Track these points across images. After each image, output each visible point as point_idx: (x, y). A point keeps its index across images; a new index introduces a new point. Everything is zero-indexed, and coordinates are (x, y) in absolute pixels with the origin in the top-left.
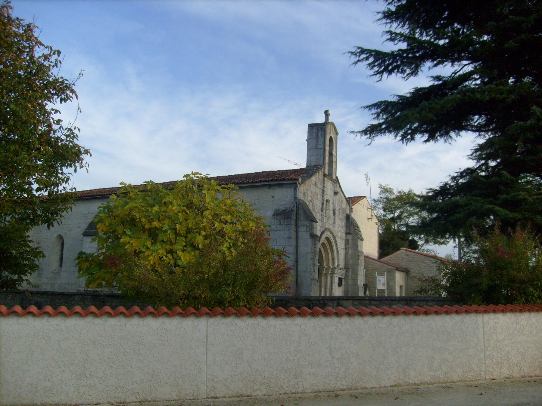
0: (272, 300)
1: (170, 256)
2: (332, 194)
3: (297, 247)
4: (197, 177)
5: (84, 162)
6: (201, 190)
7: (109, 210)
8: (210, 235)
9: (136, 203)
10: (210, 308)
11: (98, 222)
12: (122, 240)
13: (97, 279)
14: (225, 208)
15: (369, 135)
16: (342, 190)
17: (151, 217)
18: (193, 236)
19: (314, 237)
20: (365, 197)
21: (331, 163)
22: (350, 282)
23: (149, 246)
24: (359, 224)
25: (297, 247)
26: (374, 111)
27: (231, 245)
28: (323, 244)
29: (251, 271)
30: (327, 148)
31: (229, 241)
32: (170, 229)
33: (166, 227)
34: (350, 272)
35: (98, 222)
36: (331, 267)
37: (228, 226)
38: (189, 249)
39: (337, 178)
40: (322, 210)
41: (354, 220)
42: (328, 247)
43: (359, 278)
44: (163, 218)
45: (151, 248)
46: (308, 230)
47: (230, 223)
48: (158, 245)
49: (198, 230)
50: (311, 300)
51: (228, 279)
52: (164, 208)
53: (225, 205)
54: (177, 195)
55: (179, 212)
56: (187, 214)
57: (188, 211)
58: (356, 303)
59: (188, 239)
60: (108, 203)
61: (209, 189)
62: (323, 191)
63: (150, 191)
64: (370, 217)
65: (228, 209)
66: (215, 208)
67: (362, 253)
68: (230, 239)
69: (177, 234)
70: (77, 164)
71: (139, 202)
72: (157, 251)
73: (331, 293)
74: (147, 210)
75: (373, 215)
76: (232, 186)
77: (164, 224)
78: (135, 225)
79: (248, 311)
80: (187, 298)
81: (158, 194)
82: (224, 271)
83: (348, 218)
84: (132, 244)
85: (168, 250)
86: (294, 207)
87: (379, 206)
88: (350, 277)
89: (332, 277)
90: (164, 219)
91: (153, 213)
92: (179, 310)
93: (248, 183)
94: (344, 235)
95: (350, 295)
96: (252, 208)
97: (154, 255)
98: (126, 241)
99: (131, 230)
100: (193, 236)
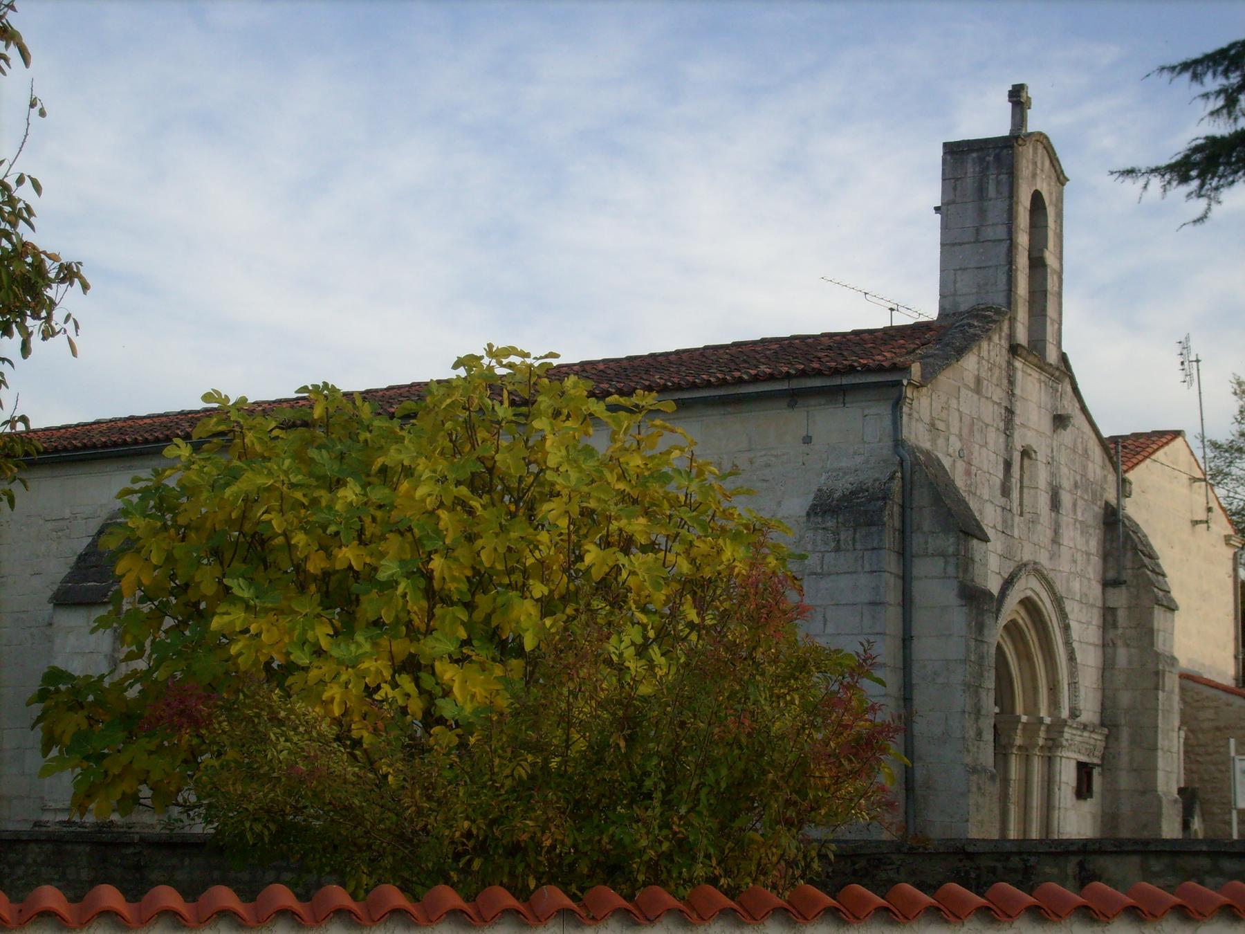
0: (822, 857)
1: (406, 681)
2: (1046, 424)
3: (907, 640)
4: (510, 366)
5: (58, 316)
6: (527, 416)
7: (161, 501)
8: (565, 599)
9: (270, 473)
10: (573, 888)
11: (122, 551)
12: (216, 623)
13: (120, 777)
14: (621, 486)
15: (1195, 184)
16: (1084, 409)
17: (332, 529)
18: (500, 600)
19: (976, 599)
20: (1177, 434)
21: (1042, 298)
22: (1125, 781)
23: (324, 643)
24: (1157, 544)
25: (907, 640)
26: (1213, 83)
27: (651, 634)
28: (1012, 629)
29: (736, 740)
30: (1023, 239)
31: (643, 618)
32: (409, 575)
33: (389, 569)
34: (1125, 734)
35: (122, 551)
36: (1048, 720)
37: (639, 560)
38: (481, 652)
39: (1064, 358)
40: (1006, 491)
41: (1136, 528)
42: (1032, 637)
43: (1161, 764)
44: (378, 531)
45: (335, 652)
46: (951, 570)
47: (644, 549)
48: (359, 638)
49: (517, 578)
50: (971, 856)
51: (646, 774)
52: (379, 494)
53: (623, 476)
54: (432, 441)
55: (441, 505)
56: (471, 512)
57: (475, 503)
58: (1156, 865)
59: (479, 615)
60: (157, 473)
61: (556, 414)
62: (1010, 412)
63: (322, 425)
64: (1201, 515)
65: (635, 493)
66: (585, 489)
67: (1173, 660)
68: (644, 610)
69: (433, 595)
70: (30, 322)
71: (282, 470)
72: (353, 664)
73: (1047, 823)
74: (315, 502)
75: (1214, 504)
76: (648, 400)
77: (382, 555)
78: (264, 561)
79: (726, 902)
80: (482, 848)
81: (353, 437)
82: (630, 740)
83: (1113, 522)
84: (258, 635)
85: (399, 658)
86: (892, 478)
87: (1234, 470)
88: (1124, 760)
89: (1050, 761)
90: (383, 538)
91: (336, 514)
92: (450, 897)
93: (708, 385)
94: (1096, 590)
95: (1125, 833)
96: (728, 485)
97: (344, 678)
98: (232, 623)
99: (251, 581)
100: (500, 600)
